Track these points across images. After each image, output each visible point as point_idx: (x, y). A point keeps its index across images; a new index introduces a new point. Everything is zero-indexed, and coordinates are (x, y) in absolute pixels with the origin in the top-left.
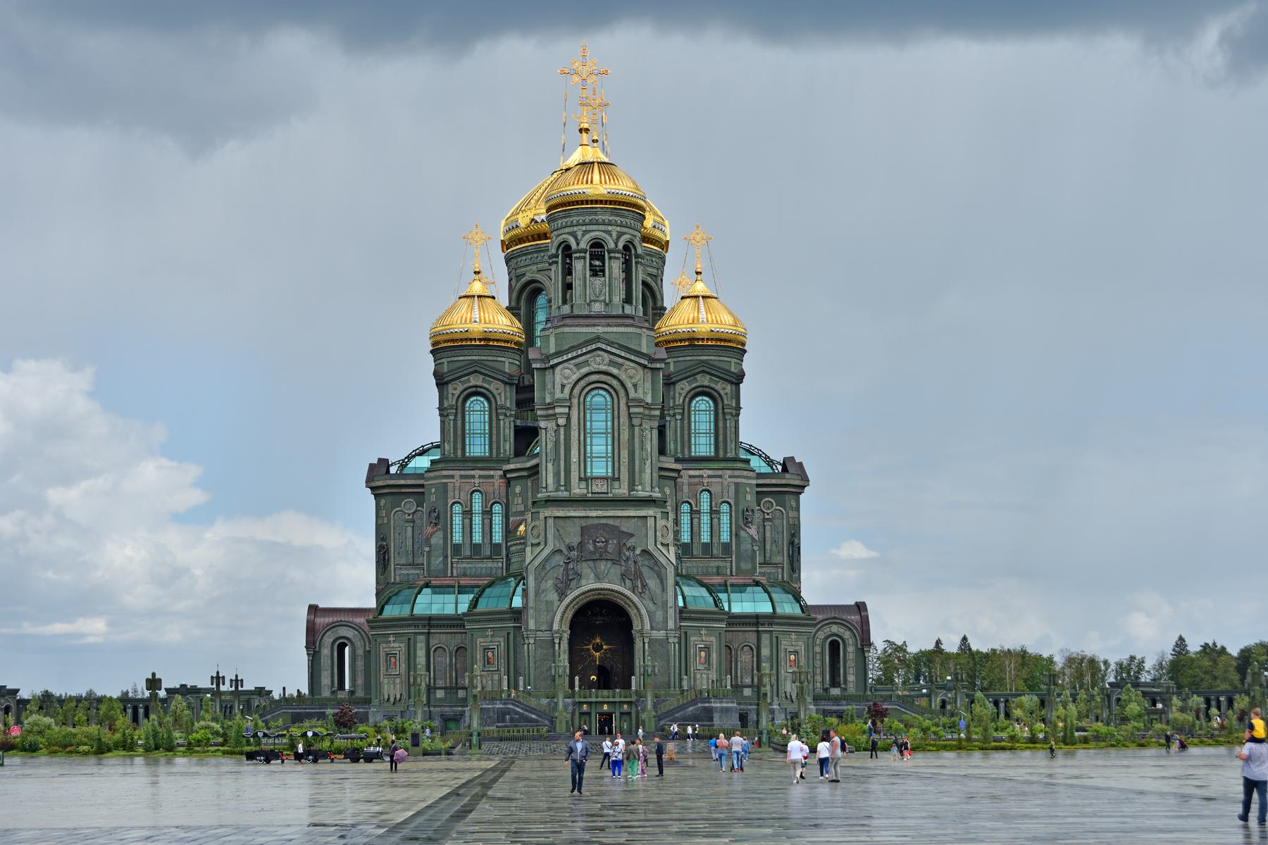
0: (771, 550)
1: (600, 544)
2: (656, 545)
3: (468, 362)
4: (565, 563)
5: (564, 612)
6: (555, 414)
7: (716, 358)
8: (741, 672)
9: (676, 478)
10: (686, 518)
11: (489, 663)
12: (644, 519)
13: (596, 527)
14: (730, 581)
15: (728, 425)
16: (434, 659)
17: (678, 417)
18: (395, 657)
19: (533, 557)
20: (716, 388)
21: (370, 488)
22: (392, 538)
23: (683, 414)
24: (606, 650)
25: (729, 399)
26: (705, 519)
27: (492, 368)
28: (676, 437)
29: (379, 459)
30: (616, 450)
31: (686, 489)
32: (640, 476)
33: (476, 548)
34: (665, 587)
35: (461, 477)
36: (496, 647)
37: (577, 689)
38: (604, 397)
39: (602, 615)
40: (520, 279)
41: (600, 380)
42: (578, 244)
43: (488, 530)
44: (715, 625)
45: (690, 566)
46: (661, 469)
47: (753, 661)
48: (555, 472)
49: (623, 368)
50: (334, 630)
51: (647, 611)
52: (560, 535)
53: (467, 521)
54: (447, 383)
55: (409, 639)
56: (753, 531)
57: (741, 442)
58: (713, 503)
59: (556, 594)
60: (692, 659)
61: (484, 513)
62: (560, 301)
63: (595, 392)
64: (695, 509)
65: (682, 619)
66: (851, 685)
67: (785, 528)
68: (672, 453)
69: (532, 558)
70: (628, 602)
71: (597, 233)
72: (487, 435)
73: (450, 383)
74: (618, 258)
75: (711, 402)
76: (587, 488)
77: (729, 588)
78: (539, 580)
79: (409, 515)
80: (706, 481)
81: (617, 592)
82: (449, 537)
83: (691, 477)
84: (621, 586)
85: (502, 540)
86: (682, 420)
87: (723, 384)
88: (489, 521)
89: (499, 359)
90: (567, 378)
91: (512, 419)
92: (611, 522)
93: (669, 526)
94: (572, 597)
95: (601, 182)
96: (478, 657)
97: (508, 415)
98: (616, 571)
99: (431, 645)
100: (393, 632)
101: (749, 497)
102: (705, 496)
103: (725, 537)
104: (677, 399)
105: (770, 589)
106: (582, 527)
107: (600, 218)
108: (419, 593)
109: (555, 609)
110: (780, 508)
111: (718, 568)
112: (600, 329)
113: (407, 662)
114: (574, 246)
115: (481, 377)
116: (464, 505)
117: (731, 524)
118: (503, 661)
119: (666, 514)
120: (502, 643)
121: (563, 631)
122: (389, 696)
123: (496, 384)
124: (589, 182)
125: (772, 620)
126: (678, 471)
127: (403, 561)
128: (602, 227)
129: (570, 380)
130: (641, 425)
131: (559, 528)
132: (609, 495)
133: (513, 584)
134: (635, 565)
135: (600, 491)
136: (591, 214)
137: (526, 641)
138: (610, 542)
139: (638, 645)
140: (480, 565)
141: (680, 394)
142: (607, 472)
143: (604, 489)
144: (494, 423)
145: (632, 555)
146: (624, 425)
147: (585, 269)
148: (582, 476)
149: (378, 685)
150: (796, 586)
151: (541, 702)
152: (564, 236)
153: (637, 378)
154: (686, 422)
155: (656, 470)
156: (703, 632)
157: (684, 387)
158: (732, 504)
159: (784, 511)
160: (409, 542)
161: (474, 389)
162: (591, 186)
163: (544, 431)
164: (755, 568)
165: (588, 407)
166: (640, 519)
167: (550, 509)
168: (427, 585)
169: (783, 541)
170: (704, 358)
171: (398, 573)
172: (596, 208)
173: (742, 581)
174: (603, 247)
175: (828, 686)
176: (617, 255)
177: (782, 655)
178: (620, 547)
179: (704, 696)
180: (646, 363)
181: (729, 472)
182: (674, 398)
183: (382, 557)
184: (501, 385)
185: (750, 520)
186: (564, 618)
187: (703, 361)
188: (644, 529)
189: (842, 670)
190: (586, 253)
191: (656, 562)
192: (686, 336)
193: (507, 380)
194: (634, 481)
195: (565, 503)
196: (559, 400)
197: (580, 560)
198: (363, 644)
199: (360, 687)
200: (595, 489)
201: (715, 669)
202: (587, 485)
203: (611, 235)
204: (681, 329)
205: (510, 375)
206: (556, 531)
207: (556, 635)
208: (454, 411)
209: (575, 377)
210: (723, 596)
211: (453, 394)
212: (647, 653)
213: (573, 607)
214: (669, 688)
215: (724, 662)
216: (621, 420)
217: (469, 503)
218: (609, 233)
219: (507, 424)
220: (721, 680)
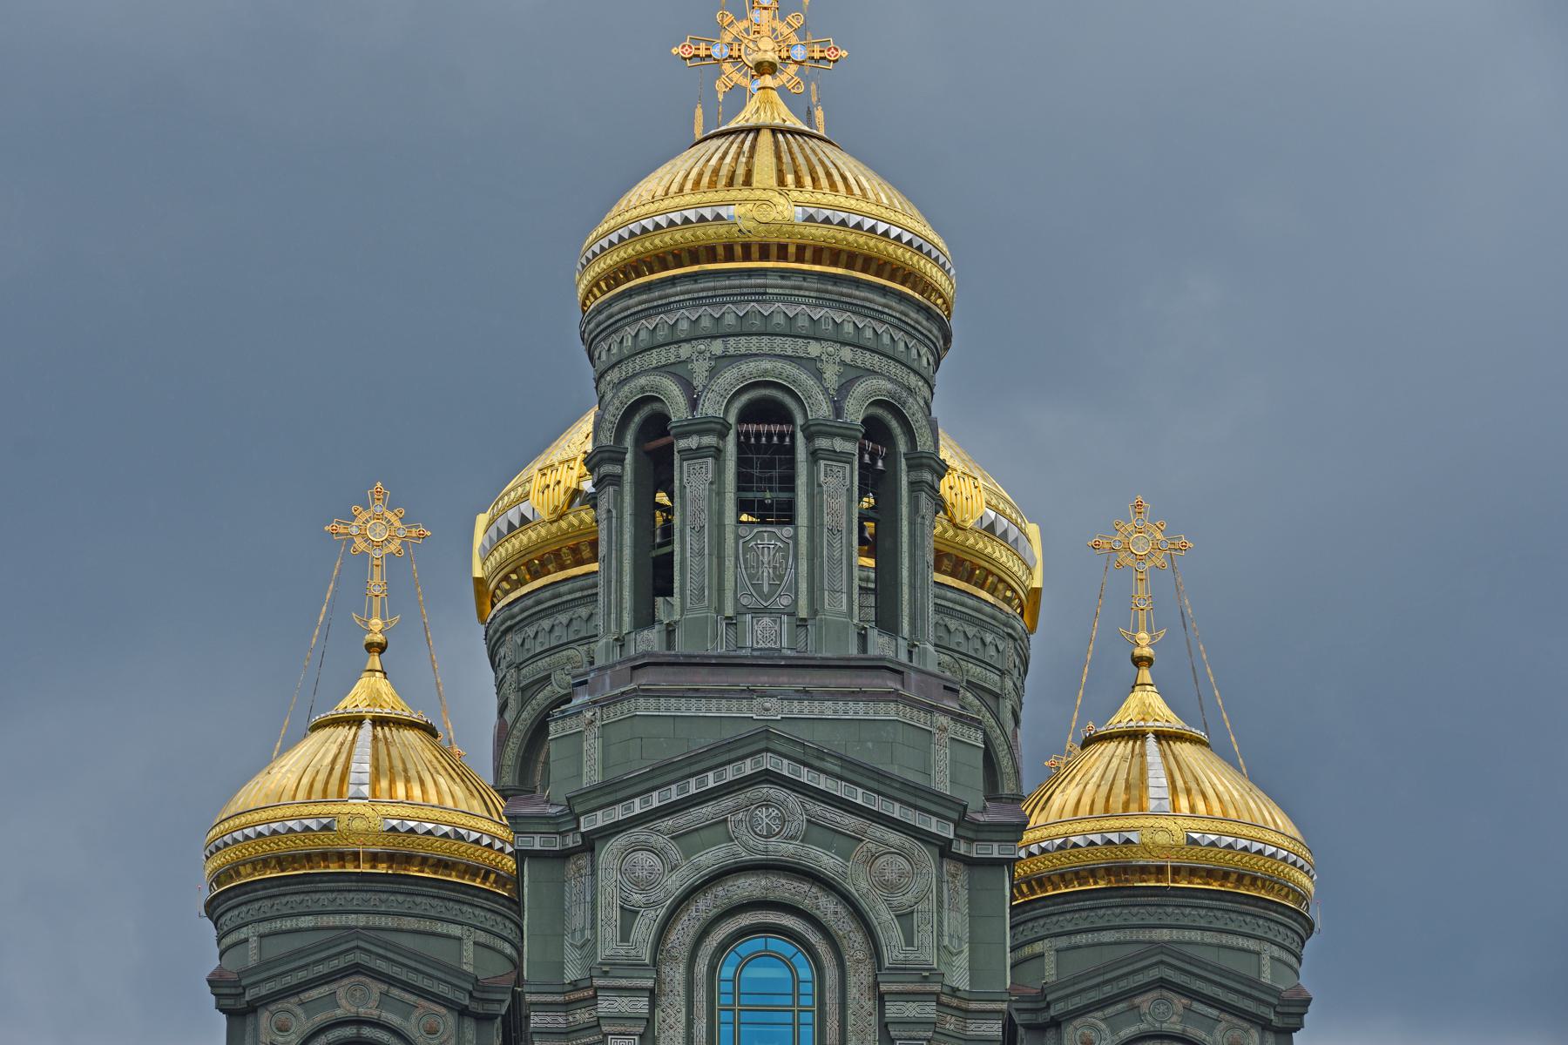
7: (1209, 937)
40: (533, 696)
41: (771, 897)
42: (693, 404)
49: (860, 851)
54: (253, 1009)
62: (627, 618)
63: (756, 944)
71: (767, 365)
74: (843, 457)
89: (441, 928)
90: (643, 885)
95: (781, 182)
107: (777, 310)
112: (774, 709)
114: (678, 410)
115: (377, 988)
128: (787, 346)
136: (742, 296)
147: (721, 494)
152: (642, 381)
153: (917, 886)
162: (746, 193)
165: (726, 1000)
170: (1165, 935)
172: (763, 272)
174: (788, 418)
176: (839, 445)
184: (447, 1021)
187: (1161, 947)
190: (723, 436)
192: (1101, 858)
203: (819, 375)
204: (1084, 834)
209: (675, 884)
218: (813, 366)
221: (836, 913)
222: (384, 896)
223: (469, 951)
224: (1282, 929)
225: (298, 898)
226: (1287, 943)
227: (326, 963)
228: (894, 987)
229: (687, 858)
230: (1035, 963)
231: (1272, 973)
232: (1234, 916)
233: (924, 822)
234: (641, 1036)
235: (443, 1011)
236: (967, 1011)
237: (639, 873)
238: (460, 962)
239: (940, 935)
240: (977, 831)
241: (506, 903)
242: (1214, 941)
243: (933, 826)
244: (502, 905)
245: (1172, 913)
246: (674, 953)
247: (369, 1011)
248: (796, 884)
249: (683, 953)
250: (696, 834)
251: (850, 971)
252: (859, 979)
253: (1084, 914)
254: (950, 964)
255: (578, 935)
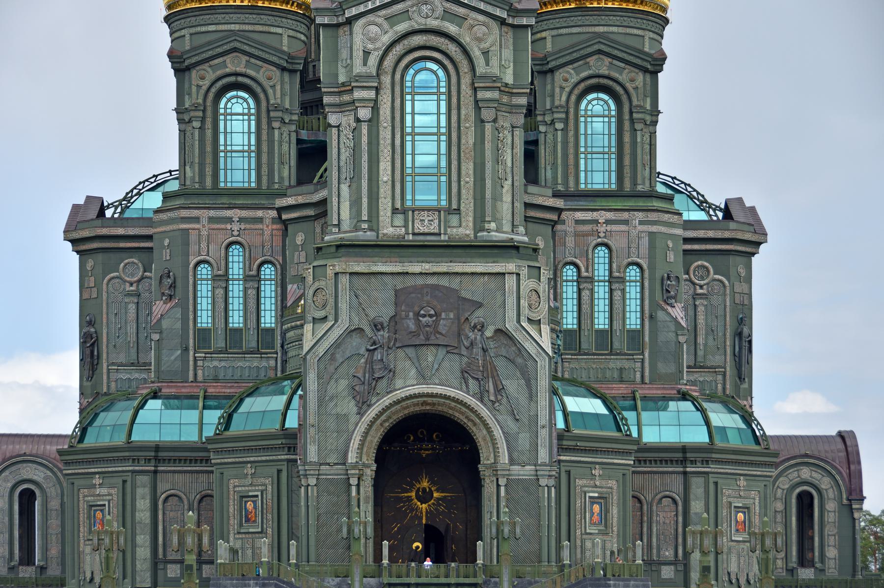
0: (705, 345)
1: (427, 319)
2: (519, 321)
3: (226, 33)
4: (368, 350)
5: (366, 433)
6: (353, 102)
7: (621, 30)
8: (658, 539)
9: (556, 223)
10: (570, 289)
11: (248, 520)
12: (499, 278)
13: (416, 289)
14: (640, 392)
15: (639, 140)
16: (164, 514)
17: (559, 126)
18: (102, 511)
19: (315, 341)
20: (620, 78)
21: (69, 241)
22: (105, 321)
23: (566, 121)
24: (438, 499)
25: (641, 96)
26: (601, 291)
27: (262, 44)
28: (556, 158)
29: (88, 198)
30: (454, 163)
31: (570, 241)
32: (494, 207)
33: (234, 336)
34: (534, 391)
35: (211, 220)
36: (259, 493)
37: (385, 561)
38: (434, 72)
39: (431, 440)
41: (428, 44)
43: (254, 308)
44: (616, 461)
45: (574, 366)
46: (528, 205)
47: (677, 521)
48: (353, 199)
49: (466, 24)
50: (13, 468)
51: (504, 433)
52: (360, 304)
53: (220, 292)
54: (188, 68)
55: (124, 482)
56: (678, 312)
57: (659, 173)
58: (614, 266)
59: (353, 403)
60: (578, 517)
61: (247, 278)
64: (584, 274)
65: (562, 449)
66: (832, 564)
67: (728, 310)
68: (549, 184)
69: (313, 343)
70: (473, 417)
72: (253, 154)
73: (194, 67)
75: (611, 103)
76: (406, 226)
77: (639, 403)
78: (324, 379)
79: (131, 284)
80: (602, 229)
81: (454, 400)
82: (191, 317)
83: (578, 222)
84: (461, 390)
85: (276, 323)
86: (565, 130)
87: (631, 72)
88: (254, 292)
89: (273, 30)
90: (373, 40)
91: (293, 128)
92: (444, 282)
93: (541, 290)
94: (380, 408)
96: (231, 510)
97: (287, 121)
98: (452, 365)
99: (159, 492)
100: (100, 470)
101: (671, 257)
102: (601, 254)
103: (633, 321)
104: (557, 98)
105: (706, 405)
106: (396, 291)
108: (142, 406)
109: (351, 428)
110: (720, 277)
111: (621, 370)
113: (121, 519)
115: (245, 58)
116: (215, 265)
117: (642, 299)
118: (269, 517)
119: (536, 271)
120: (269, 488)
121: (364, 465)
122: (92, 573)
123: (268, 70)
124: (532, 213)
125: (709, 455)
126: (559, 211)
127: (122, 359)
129: (378, 45)
130: (495, 121)
131: (359, 292)
132: (443, 237)
133: (288, 391)
134: (484, 355)
135: (426, 231)
137: (303, 482)
138: (443, 315)
139: (488, 488)
140: (240, 364)
141: (562, 88)
142: (439, 200)
143: (434, 228)
144: (264, 133)
145: (478, 337)
146: (466, 120)
148: (398, 205)
149: (76, 556)
150: (745, 403)
151: (326, 584)
153: (490, 40)
154: (571, 133)
155: (519, 206)
156: (596, 472)
157: (568, 77)
158: (645, 266)
159: (726, 282)
160: (132, 329)
161: (232, 79)
163: (335, 131)
164: (681, 372)
166: (493, 278)
167: (343, 259)
168: (155, 395)
169: (725, 329)
170: (601, 29)
171: (113, 376)
173: (659, 392)
175: (795, 565)
177: (724, 512)
178: (461, 323)
179: (597, 576)
180: (504, 15)
181: (640, 215)
182: (552, 96)
183: (88, 351)
184: (276, 73)
185: (672, 293)
186: (366, 444)
188: (499, 294)
189: (816, 539)
191: (519, 350)
193: (285, 65)
194: (483, 216)
195: (370, 250)
196: (359, 77)
197: (395, 345)
198: (59, 491)
199: (54, 561)
200: (420, 228)
201: (615, 533)
202: (406, 221)
205: (289, 55)
206: (354, 298)
207: (353, 472)
208: (200, 114)
209: (386, 39)
210: (630, 416)
211: (199, 87)
212: (503, 503)
213: (381, 425)
214: (540, 561)
215: (630, 520)
216: (463, 112)
217: (223, 263)
219: (285, 135)
220: (627, 549)
221: (456, 51)
222: (247, 16)
223: (285, 40)
224: (654, 24)
225: (208, 17)
226: (656, 31)
227: (221, 47)
228: (481, 85)
229: (391, 28)
230: (543, 40)
231: (649, 46)
232: (632, 19)
233: (494, 11)
234: (372, 107)
235: (275, 69)
236: (512, 93)
237: (371, 35)
238: (282, 45)
239: (501, 60)
240: (517, 13)
241: (302, 16)
242: (623, 32)
243: (498, 12)
244: (300, 17)
245: (604, 19)
246: (386, 70)
247: (241, 69)
248: (438, 39)
249: (390, 70)
250: (395, 17)
251: (462, 78)
252: (466, 81)
253: (565, 19)
254: (505, 73)
255: (344, 62)
